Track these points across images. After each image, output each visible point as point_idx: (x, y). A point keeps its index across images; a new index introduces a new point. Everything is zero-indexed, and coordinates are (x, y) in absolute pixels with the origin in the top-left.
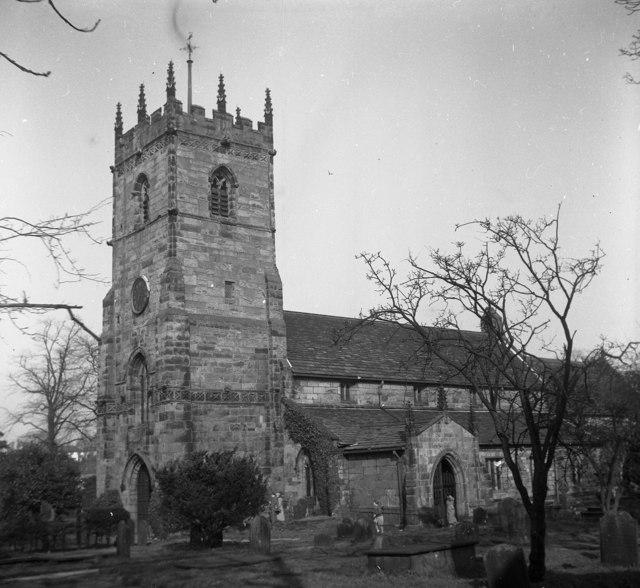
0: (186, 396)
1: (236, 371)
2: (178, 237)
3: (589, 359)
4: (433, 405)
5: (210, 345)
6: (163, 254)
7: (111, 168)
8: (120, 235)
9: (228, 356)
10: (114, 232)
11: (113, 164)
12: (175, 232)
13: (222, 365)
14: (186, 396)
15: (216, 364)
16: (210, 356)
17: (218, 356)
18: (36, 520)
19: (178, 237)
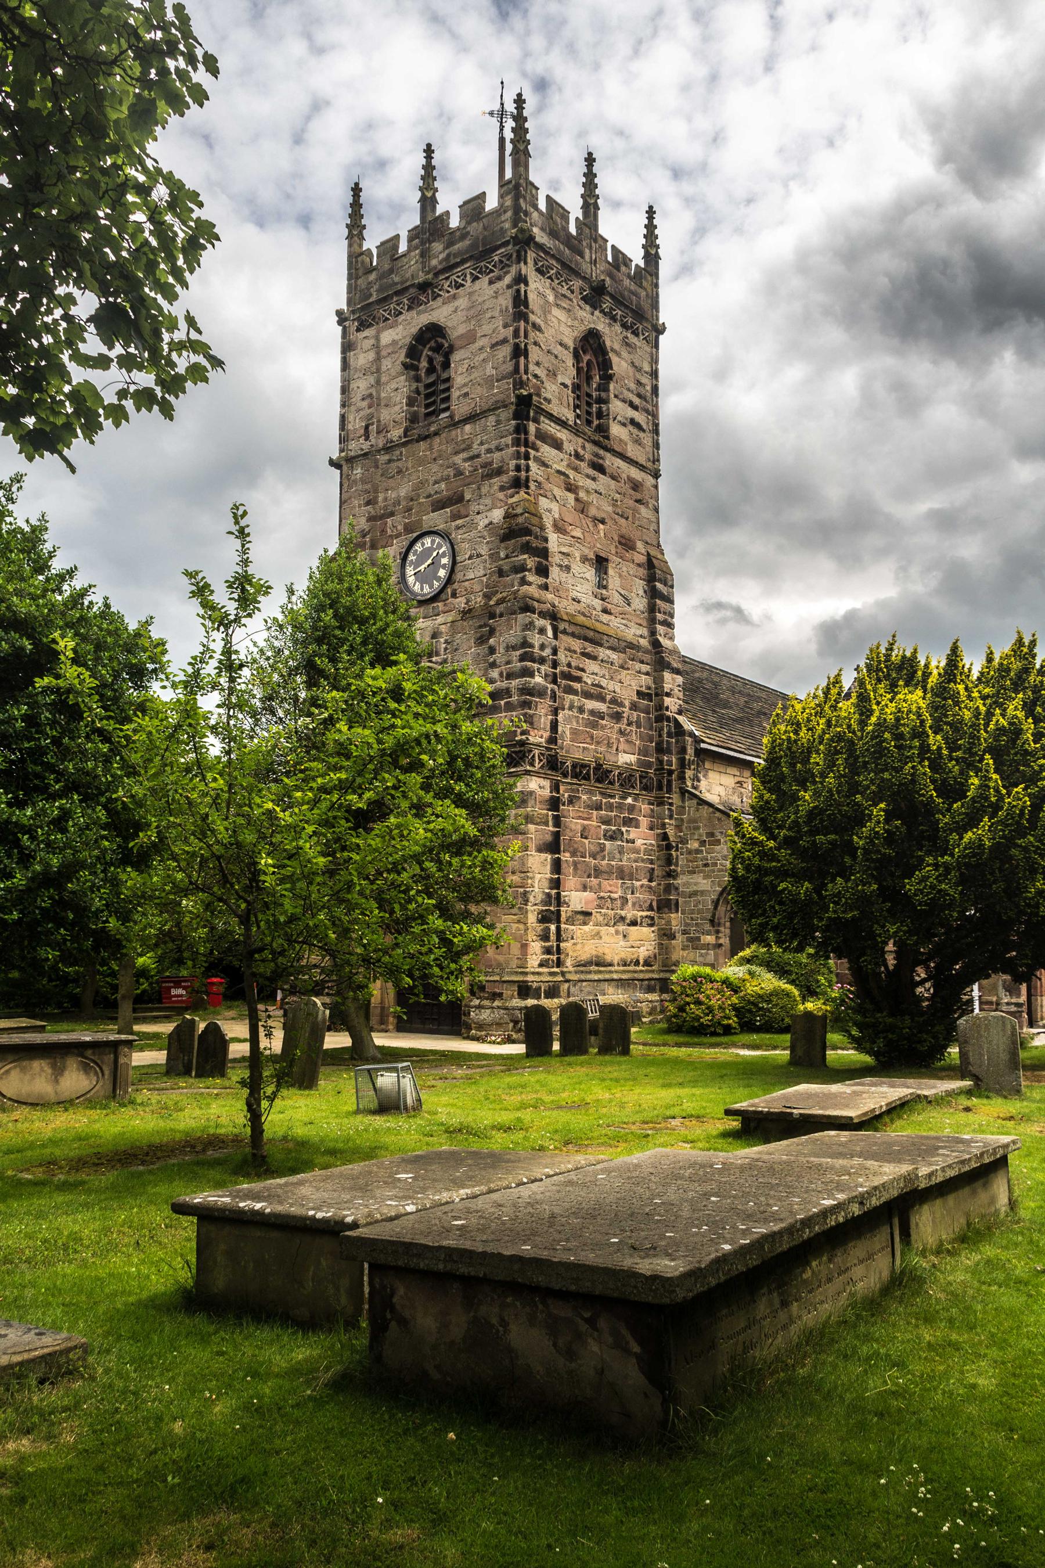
0: (553, 764)
1: (610, 729)
2: (532, 452)
3: (298, 606)
4: (243, 906)
5: (576, 673)
6: (497, 482)
7: (339, 313)
8: (356, 446)
9: (601, 698)
10: (343, 440)
11: (344, 307)
12: (526, 440)
13: (592, 712)
14: (553, 764)
15: (581, 710)
16: (575, 692)
17: (588, 695)
18: (454, 890)
19: (532, 452)
